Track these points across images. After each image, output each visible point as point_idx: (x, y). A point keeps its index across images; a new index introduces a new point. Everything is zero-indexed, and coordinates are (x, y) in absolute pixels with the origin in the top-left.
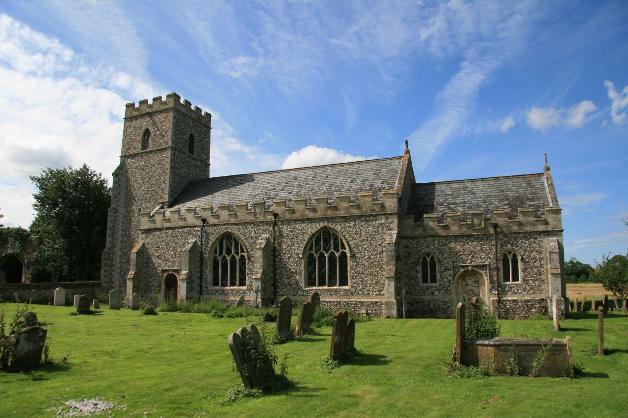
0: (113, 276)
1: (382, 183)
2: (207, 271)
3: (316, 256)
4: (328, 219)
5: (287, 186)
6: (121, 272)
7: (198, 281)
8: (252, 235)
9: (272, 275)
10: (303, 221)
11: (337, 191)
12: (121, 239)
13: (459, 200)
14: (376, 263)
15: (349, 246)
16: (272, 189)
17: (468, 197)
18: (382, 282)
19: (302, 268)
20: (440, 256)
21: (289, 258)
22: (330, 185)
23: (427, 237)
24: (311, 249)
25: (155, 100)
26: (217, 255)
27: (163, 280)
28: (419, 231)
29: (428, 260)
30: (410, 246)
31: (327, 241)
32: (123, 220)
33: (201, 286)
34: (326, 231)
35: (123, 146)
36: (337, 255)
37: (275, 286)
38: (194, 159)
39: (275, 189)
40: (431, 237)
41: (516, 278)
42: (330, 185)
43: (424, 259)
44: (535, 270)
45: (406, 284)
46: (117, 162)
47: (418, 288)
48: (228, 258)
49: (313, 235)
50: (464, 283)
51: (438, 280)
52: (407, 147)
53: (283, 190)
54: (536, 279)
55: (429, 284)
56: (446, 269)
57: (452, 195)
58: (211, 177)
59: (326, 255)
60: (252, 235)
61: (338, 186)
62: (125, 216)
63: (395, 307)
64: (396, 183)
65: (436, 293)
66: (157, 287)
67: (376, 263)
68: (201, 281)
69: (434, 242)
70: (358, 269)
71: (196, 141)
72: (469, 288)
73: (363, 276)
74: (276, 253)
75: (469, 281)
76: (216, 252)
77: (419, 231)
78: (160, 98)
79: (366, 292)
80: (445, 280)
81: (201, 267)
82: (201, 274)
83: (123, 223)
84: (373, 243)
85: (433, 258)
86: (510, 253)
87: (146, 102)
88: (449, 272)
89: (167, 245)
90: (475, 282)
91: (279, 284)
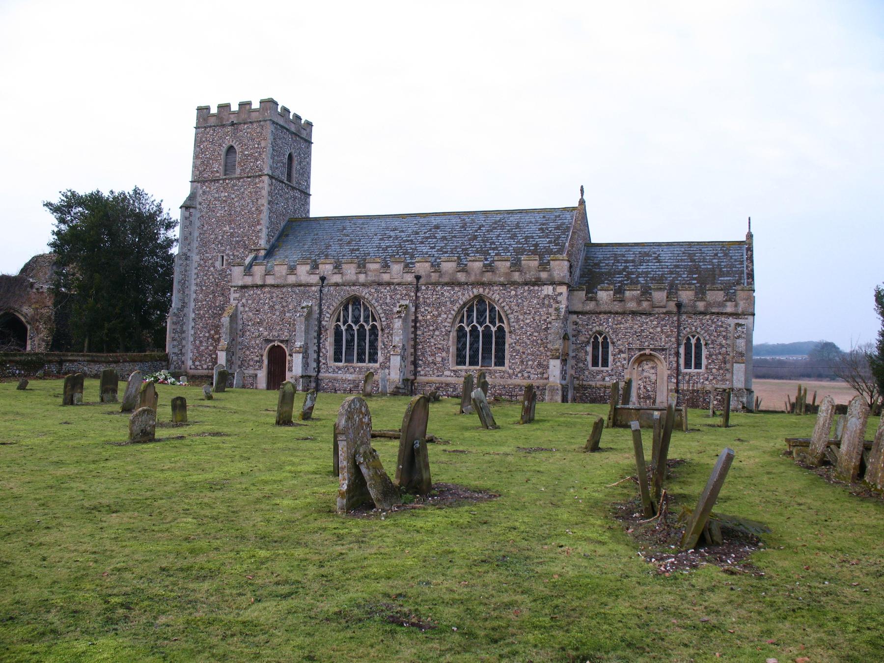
0: (183, 346)
1: (550, 242)
2: (327, 344)
3: (468, 329)
4: (483, 284)
5: (427, 238)
6: (195, 341)
7: (315, 356)
8: (388, 301)
9: (412, 350)
10: (453, 284)
11: (494, 249)
12: (194, 296)
13: (642, 269)
14: (539, 341)
15: (508, 319)
16: (408, 241)
17: (653, 266)
18: (545, 363)
19: (450, 343)
20: (613, 337)
21: (434, 330)
22: (484, 241)
23: (600, 313)
24: (461, 321)
25: (242, 105)
26: (340, 324)
27: (265, 354)
28: (591, 306)
29: (600, 339)
30: (580, 322)
31: (356, 308)
32: (196, 271)
33: (318, 362)
34: (480, 299)
35: (195, 166)
36: (493, 329)
37: (415, 364)
38: (293, 188)
39: (411, 241)
40: (605, 313)
41: (698, 365)
42: (484, 241)
43: (596, 338)
44: (720, 357)
45: (572, 367)
46: (187, 192)
47: (587, 373)
48: (355, 328)
49: (465, 304)
50: (640, 369)
51: (610, 364)
52: (582, 195)
53: (422, 243)
54: (720, 368)
55: (600, 368)
56: (621, 352)
57: (633, 261)
58: (313, 214)
59: (480, 329)
60: (388, 301)
61: (493, 243)
62: (199, 265)
63: (560, 392)
64: (567, 244)
65: (607, 379)
66: (257, 361)
67: (539, 341)
68: (319, 356)
69: (608, 320)
70: (518, 348)
71: (295, 163)
72: (645, 374)
73: (524, 356)
74: (418, 325)
75: (646, 367)
76: (338, 320)
77: (591, 306)
78: (249, 103)
79: (526, 375)
80: (619, 364)
81: (319, 337)
82: (319, 347)
83: (197, 274)
84: (537, 318)
85: (605, 338)
86: (693, 336)
87: (227, 106)
88: (623, 355)
89: (272, 308)
90: (653, 368)
91: (420, 362)
